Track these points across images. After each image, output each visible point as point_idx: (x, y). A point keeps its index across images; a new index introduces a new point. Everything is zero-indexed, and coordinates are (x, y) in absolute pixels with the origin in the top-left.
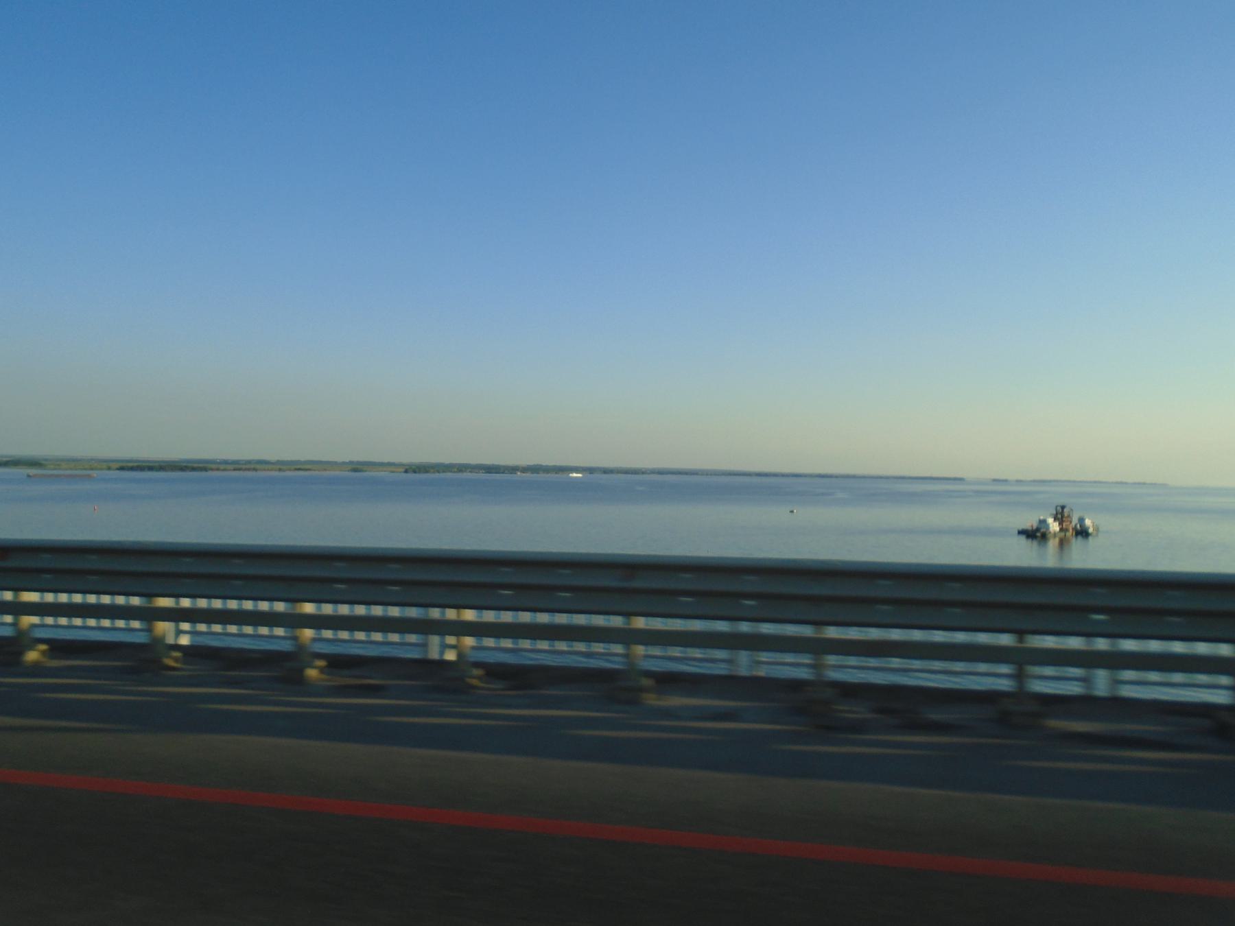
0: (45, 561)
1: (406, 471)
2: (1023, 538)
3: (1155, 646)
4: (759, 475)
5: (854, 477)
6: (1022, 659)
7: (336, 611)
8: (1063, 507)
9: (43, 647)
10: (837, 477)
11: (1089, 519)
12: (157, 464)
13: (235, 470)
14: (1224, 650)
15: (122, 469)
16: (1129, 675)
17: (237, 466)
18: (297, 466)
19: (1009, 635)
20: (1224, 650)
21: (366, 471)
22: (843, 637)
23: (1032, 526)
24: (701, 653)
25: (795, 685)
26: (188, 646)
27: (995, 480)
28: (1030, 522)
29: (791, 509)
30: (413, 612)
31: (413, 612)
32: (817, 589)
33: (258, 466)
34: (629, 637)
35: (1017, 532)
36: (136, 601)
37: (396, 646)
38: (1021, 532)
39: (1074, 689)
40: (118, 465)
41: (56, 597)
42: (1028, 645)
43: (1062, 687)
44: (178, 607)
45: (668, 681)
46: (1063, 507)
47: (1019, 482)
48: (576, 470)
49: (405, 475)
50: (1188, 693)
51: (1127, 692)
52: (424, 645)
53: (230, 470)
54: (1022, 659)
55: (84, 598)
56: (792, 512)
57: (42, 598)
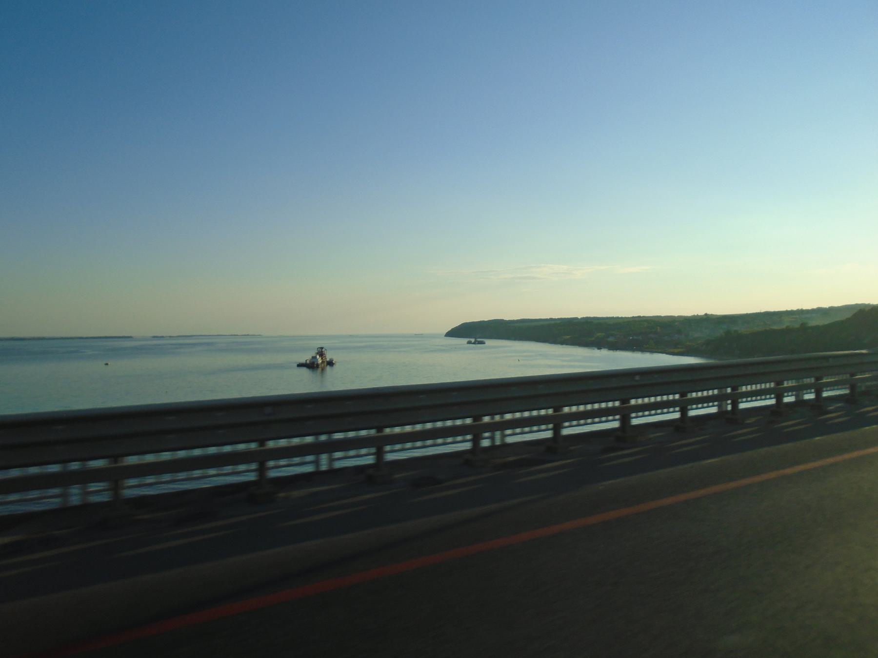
2: (304, 370)
3: (166, 456)
4: (13, 339)
5: (43, 339)
6: (379, 444)
7: (578, 409)
16: (338, 454)
19: (152, 454)
22: (6, 477)
24: (284, 461)
26: (716, 413)
27: (154, 337)
28: (306, 358)
35: (296, 365)
36: (309, 439)
37: (36, 501)
38: (300, 365)
39: (309, 469)
41: (570, 409)
42: (125, 464)
43: (353, 462)
44: (504, 420)
46: (322, 348)
50: (175, 486)
51: (338, 465)
54: (261, 458)
57: (570, 409)
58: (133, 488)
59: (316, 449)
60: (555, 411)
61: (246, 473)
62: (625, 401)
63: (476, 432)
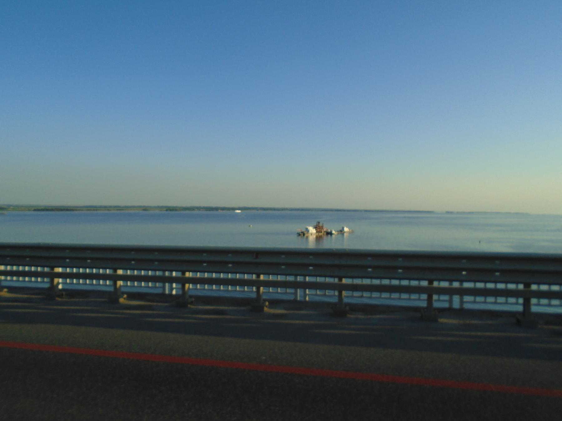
0: (28, 253)
1: (167, 210)
6: (115, 278)
8: (319, 223)
9: (5, 290)
10: (344, 211)
11: (347, 227)
12: (51, 208)
13: (87, 210)
14: (555, 288)
15: (35, 210)
17: (89, 209)
18: (118, 208)
19: (266, 275)
20: (555, 288)
21: (110, 210)
23: (301, 231)
25: (417, 309)
29: (249, 225)
30: (291, 278)
31: (291, 278)
32: (337, 262)
33: (110, 209)
34: (258, 284)
40: (33, 209)
45: (274, 303)
47: (458, 213)
48: (239, 209)
49: (165, 212)
52: (296, 294)
53: (85, 210)
54: (430, 292)
55: (390, 282)
56: (250, 226)
58: (348, 297)
59: (295, 285)
60: (525, 287)
61: (420, 301)
62: (527, 285)
63: (527, 296)
